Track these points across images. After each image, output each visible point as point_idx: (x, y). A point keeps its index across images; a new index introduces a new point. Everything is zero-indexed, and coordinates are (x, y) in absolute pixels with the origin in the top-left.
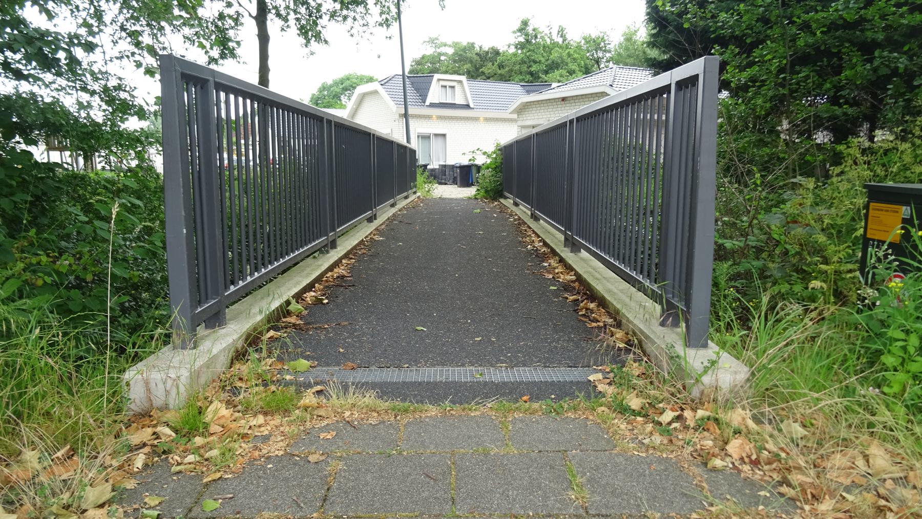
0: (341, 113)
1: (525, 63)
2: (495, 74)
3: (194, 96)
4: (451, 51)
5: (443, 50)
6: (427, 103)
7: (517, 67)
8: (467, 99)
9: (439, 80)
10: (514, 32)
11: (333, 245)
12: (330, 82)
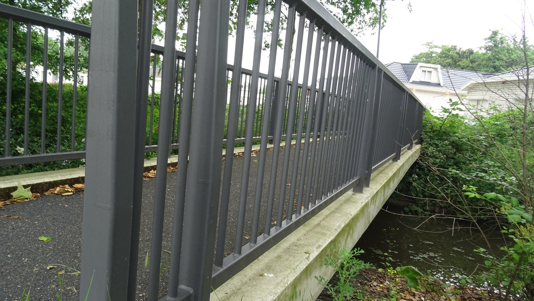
1: (491, 60)
2: (468, 67)
3: (198, 31)
4: (439, 51)
5: (435, 50)
6: (411, 81)
7: (484, 62)
8: (439, 80)
9: (421, 67)
10: (486, 39)
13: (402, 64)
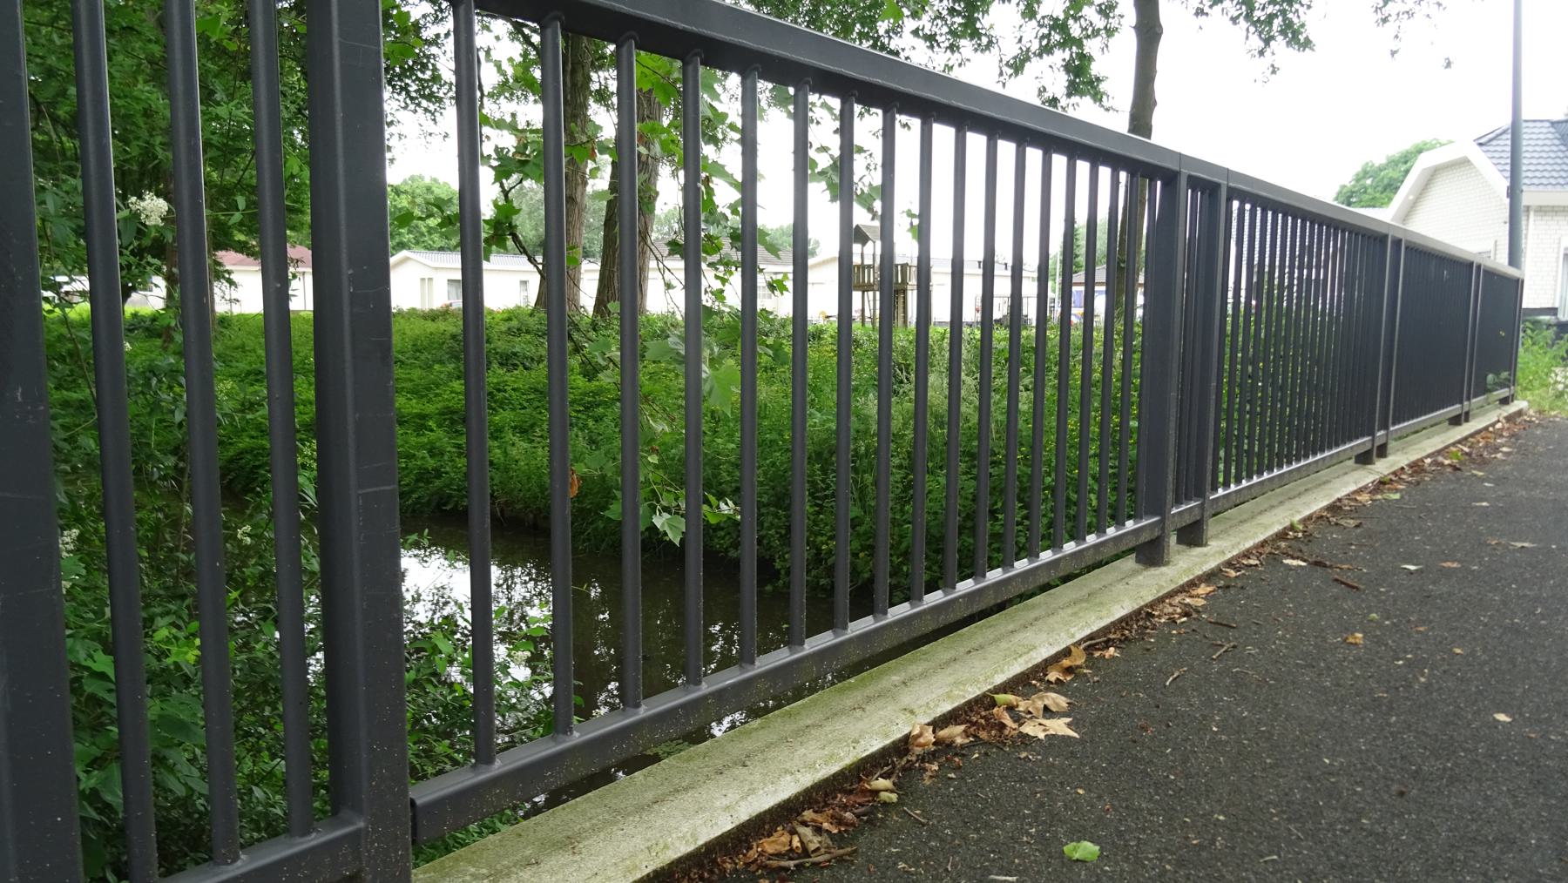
0: (1384, 215)
11: (1382, 451)
12: (1379, 160)
13: (1553, 124)
